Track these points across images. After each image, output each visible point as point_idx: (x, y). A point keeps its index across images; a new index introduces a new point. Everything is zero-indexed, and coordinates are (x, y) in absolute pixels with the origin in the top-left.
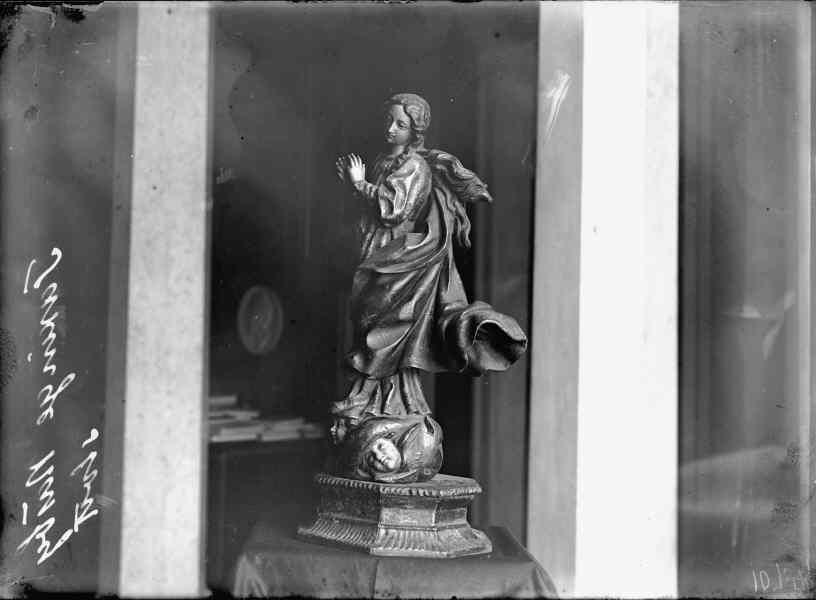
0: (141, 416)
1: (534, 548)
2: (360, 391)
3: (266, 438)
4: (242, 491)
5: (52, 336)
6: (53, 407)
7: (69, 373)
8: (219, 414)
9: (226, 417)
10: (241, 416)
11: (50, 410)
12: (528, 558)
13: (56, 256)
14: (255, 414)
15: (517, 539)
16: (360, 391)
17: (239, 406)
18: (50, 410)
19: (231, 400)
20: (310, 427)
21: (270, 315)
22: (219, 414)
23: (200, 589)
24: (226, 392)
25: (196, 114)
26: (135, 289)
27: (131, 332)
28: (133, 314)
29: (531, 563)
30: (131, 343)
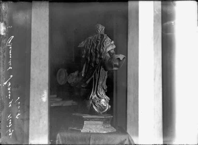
0: (34, 100)
1: (128, 131)
2: (95, 37)
3: (64, 105)
4: (58, 119)
5: (11, 60)
6: (10, 94)
7: (12, 36)
8: (52, 99)
9: (54, 100)
10: (58, 100)
11: (10, 105)
12: (127, 133)
13: (10, 65)
14: (61, 99)
15: (124, 129)
16: (95, 37)
17: (57, 97)
18: (10, 105)
19: (55, 96)
20: (74, 102)
21: (64, 75)
22: (52, 99)
23: (48, 143)
24: (54, 94)
25: (46, 27)
26: (32, 70)
27: (31, 80)
28: (31, 76)
29: (128, 135)
30: (31, 82)
